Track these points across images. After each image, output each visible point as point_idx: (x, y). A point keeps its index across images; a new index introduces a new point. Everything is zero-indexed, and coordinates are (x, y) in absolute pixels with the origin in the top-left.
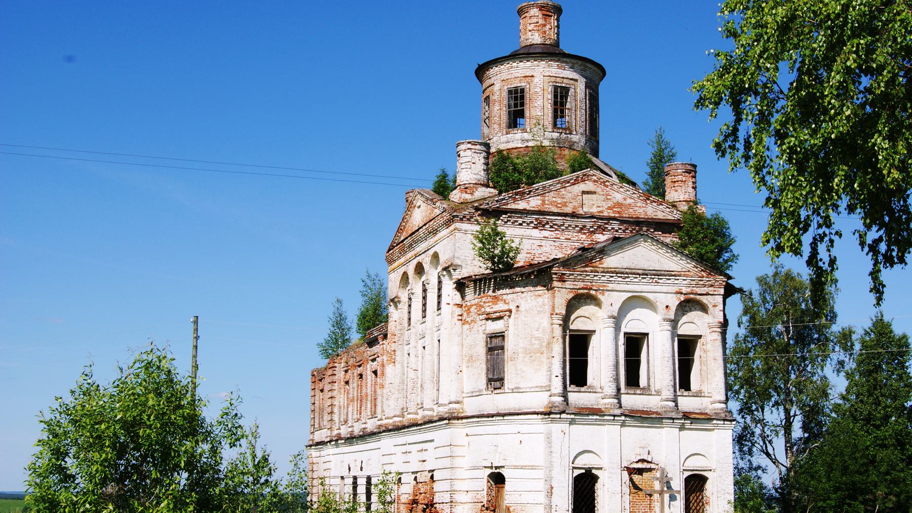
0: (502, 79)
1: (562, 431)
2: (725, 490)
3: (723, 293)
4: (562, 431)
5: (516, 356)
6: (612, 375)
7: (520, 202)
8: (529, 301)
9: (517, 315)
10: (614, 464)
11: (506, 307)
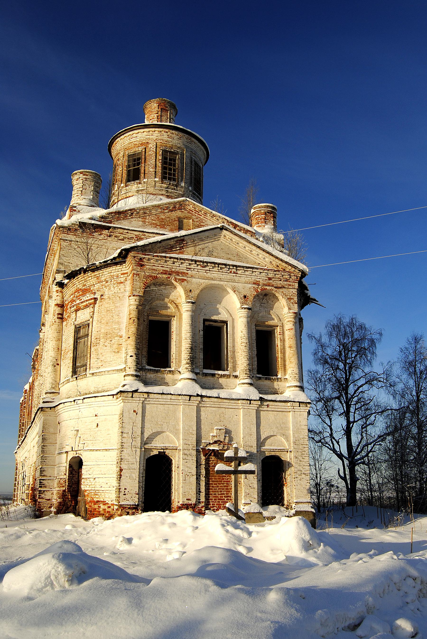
0: (345, 566)
1: (134, 411)
2: (301, 471)
3: (297, 288)
4: (134, 411)
5: (98, 342)
6: (189, 357)
7: (123, 221)
8: (112, 289)
9: (101, 303)
10: (189, 445)
11: (92, 296)
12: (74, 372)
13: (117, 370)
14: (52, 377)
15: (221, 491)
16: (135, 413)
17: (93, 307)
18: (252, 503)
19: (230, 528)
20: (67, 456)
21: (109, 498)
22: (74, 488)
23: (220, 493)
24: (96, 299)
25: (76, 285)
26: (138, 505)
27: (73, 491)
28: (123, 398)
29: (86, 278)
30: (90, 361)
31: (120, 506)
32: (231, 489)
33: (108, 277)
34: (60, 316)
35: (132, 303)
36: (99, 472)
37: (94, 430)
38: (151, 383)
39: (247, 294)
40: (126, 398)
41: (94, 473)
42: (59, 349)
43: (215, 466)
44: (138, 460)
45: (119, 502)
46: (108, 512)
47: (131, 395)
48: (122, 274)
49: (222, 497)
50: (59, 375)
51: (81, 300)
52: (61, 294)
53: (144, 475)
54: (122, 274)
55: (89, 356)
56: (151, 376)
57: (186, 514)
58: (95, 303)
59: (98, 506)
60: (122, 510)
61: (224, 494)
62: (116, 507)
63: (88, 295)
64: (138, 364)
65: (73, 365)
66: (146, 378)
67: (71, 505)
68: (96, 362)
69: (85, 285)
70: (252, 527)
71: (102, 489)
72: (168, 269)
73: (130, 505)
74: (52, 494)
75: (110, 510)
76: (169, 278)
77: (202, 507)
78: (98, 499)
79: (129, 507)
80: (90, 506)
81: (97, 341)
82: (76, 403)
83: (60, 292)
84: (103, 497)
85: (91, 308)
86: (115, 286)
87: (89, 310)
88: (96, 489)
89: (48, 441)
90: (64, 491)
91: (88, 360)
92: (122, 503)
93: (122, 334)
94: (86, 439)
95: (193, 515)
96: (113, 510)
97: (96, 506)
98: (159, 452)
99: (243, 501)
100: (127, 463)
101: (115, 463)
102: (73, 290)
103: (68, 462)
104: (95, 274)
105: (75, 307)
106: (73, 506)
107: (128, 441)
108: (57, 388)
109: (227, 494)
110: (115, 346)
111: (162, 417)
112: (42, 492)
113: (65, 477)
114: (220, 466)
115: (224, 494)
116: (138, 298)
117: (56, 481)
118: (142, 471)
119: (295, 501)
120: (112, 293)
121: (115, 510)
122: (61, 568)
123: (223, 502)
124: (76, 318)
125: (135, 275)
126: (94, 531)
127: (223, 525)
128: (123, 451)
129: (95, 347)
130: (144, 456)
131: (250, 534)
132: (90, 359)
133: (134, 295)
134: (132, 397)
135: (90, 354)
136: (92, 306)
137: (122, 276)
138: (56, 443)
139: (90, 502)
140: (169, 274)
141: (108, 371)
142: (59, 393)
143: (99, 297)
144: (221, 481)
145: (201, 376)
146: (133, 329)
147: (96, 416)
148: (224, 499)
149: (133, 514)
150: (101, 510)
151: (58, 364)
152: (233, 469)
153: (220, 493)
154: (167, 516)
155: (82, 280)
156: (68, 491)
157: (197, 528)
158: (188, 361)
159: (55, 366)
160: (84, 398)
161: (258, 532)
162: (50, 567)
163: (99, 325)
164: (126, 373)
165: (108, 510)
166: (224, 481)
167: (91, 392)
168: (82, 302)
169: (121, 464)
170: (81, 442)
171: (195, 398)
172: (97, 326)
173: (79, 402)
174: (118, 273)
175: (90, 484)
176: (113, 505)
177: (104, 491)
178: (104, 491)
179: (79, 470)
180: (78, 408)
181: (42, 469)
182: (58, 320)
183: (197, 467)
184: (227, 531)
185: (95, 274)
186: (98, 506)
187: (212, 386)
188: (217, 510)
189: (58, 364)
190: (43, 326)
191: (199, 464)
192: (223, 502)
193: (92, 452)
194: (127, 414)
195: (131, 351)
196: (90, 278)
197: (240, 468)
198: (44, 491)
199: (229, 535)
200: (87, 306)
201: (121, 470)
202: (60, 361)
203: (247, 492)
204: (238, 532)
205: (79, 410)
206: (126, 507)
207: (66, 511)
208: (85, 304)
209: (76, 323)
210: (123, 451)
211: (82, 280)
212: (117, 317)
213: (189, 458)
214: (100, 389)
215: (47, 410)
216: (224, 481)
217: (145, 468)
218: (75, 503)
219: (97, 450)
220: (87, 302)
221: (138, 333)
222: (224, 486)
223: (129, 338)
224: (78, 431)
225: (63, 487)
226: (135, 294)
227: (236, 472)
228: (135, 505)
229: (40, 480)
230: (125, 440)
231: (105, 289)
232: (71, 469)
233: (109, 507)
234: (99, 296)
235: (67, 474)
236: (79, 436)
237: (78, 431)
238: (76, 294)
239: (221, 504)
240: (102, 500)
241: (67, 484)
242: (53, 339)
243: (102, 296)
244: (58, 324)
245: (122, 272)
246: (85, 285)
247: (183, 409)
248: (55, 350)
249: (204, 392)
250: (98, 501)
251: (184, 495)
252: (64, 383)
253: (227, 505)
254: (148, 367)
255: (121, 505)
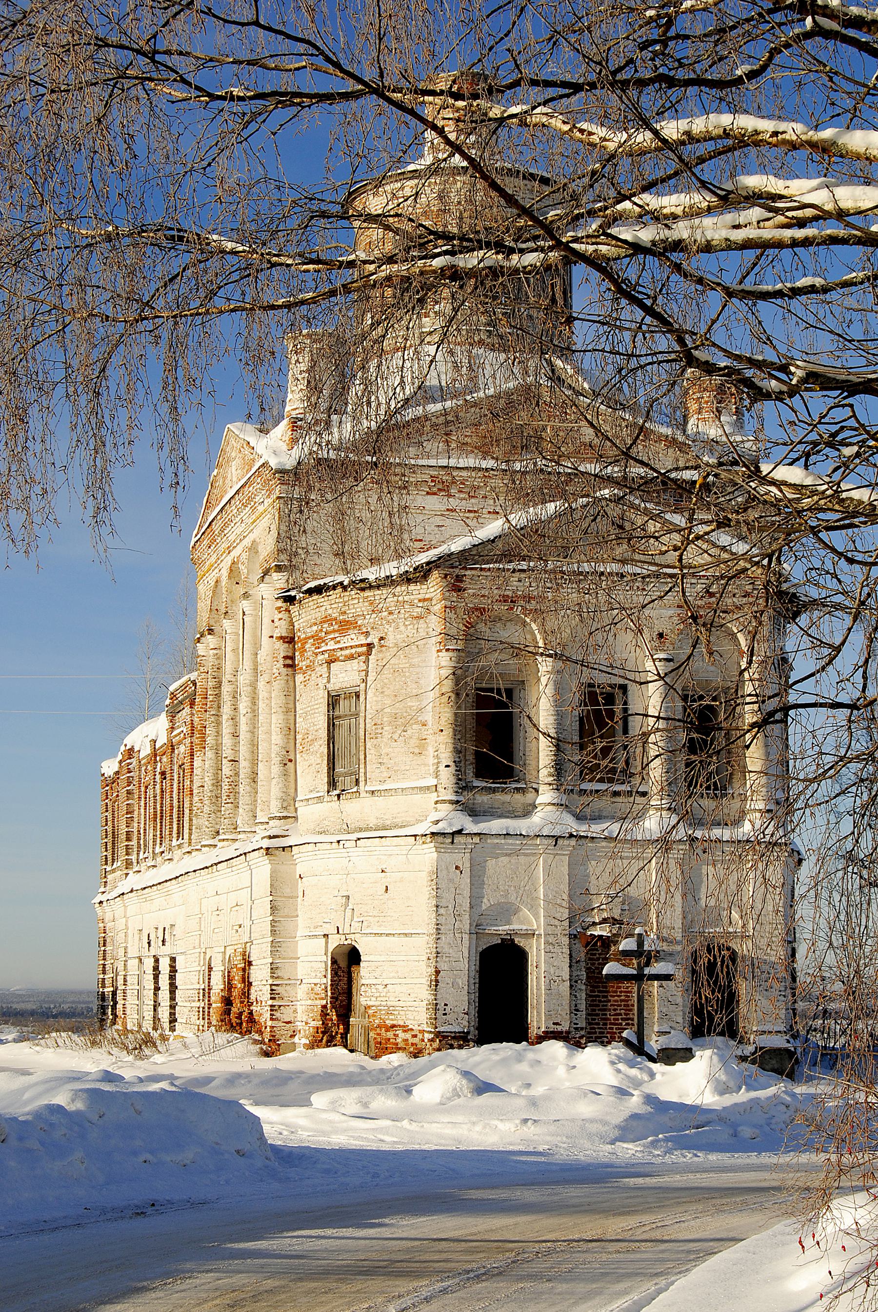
4: (457, 868)
5: (380, 731)
9: (381, 655)
10: (556, 926)
12: (332, 783)
13: (421, 788)
14: (280, 785)
15: (615, 1010)
16: (458, 872)
17: (367, 662)
18: (672, 1031)
19: (621, 1066)
20: (327, 943)
21: (414, 1020)
22: (341, 1002)
23: (613, 1012)
24: (370, 646)
25: (324, 608)
26: (468, 1033)
27: (340, 1006)
28: (437, 845)
29: (346, 599)
30: (365, 767)
31: (438, 1034)
32: (633, 1005)
33: (393, 604)
34: (289, 662)
35: (443, 664)
36: (392, 975)
37: (381, 897)
38: (484, 812)
39: (665, 630)
40: (442, 846)
41: (384, 975)
42: (291, 731)
43: (602, 969)
44: (466, 954)
45: (436, 1028)
46: (412, 1044)
47: (450, 840)
48: (420, 601)
49: (618, 1019)
50: (293, 782)
51: (339, 642)
52: (287, 615)
53: (477, 981)
54: (420, 601)
55: (362, 757)
56: (483, 799)
57: (556, 1048)
58: (369, 653)
59: (394, 1035)
60: (440, 1041)
61: (620, 1014)
62: (428, 1036)
63: (353, 636)
64: (460, 780)
65: (329, 769)
66: (474, 804)
67: (337, 1033)
68: (377, 771)
69: (345, 612)
70: (656, 1067)
71: (401, 1004)
72: (509, 593)
73: (455, 1032)
74: (295, 1011)
75: (415, 1040)
76: (512, 609)
77: (581, 1037)
78: (395, 1022)
79: (453, 1035)
80: (379, 1034)
81: (376, 729)
82: (341, 846)
83: (286, 610)
84: (404, 1017)
85: (362, 663)
86: (407, 623)
87: (356, 665)
88: (389, 1003)
89: (282, 911)
90: (324, 1007)
91: (362, 766)
92: (442, 1029)
93: (426, 719)
94: (366, 914)
95: (567, 1048)
96: (423, 1040)
97: (390, 1034)
98: (502, 939)
99: (656, 1029)
100: (447, 959)
101: (425, 958)
102: (319, 615)
103: (329, 955)
104: (366, 595)
105: (326, 655)
106: (341, 1034)
107: (448, 921)
108: (292, 808)
109: (626, 1014)
110: (414, 742)
111: (507, 877)
112: (277, 1007)
113: (324, 981)
114: (610, 968)
115: (620, 1014)
116: (455, 654)
117: (304, 987)
118: (473, 974)
119: (755, 1029)
120: (402, 636)
121: (426, 1040)
122: (464, 1082)
123: (619, 1029)
124: (329, 677)
125: (448, 610)
126: (399, 1074)
127: (613, 1063)
128: (439, 938)
129: (375, 741)
130: (477, 947)
131: (652, 1075)
132: (365, 762)
133: (447, 650)
134: (452, 843)
135: (365, 754)
136: (363, 658)
137: (420, 604)
138: (297, 916)
139: (379, 1026)
140: (512, 601)
141: (403, 789)
142: (296, 818)
143: (376, 641)
144: (616, 992)
145: (576, 796)
146: (447, 715)
147: (383, 871)
148: (621, 1024)
149: (460, 1047)
150: (399, 1040)
151: (290, 761)
152: (635, 972)
153: (613, 1012)
154: (525, 1050)
155: (337, 600)
156: (333, 1007)
157: (574, 1067)
158: (552, 770)
159: (285, 764)
160: (359, 839)
161: (663, 1074)
162: (455, 1081)
163: (379, 699)
164: (438, 796)
165: (411, 1040)
166: (621, 992)
167: (371, 825)
168: (341, 649)
169: (437, 962)
170: (356, 919)
171: (566, 842)
172: (375, 699)
173: (348, 844)
174: (412, 597)
175: (378, 994)
176: (422, 1032)
177: (405, 1009)
178: (405, 1009)
179: (349, 967)
180: (346, 855)
181: (274, 966)
182: (284, 671)
183: (570, 967)
184: (619, 1071)
185: (366, 595)
186: (394, 1035)
187: (597, 814)
188: (609, 1043)
189: (290, 761)
190: (209, 634)
191: (574, 961)
192: (619, 1029)
193: (378, 938)
194: (445, 872)
195: (446, 756)
196: (356, 601)
197: (647, 971)
198: (280, 1006)
199: (621, 1075)
200: (351, 657)
201: (437, 972)
202: (293, 753)
203: (664, 1011)
204: (634, 1072)
205: (348, 859)
206: (448, 1036)
207: (330, 1043)
208: (347, 652)
209: (330, 687)
210: (439, 938)
211: (337, 600)
212: (414, 686)
213: (557, 949)
214: (388, 822)
215: (277, 852)
216: (621, 992)
217: (478, 968)
218: (344, 1029)
219: (387, 935)
220: (353, 651)
221: (456, 720)
222: (622, 1001)
223: (442, 731)
224: (348, 897)
225: (323, 999)
226: (450, 647)
227: (639, 978)
228: (463, 1032)
229: (271, 985)
230: (442, 920)
231: (387, 627)
232: (336, 966)
233: (415, 1036)
234: (377, 640)
235: (329, 976)
236: (351, 907)
237: (348, 897)
238: (326, 625)
239: (615, 1033)
240: (402, 1023)
241: (329, 994)
242: (279, 709)
243: (382, 639)
244: (286, 678)
245: (420, 596)
246: (345, 612)
247: (545, 861)
248: (284, 733)
249: (582, 829)
250: (393, 1026)
251: (548, 1016)
252: (310, 802)
253: (624, 1035)
254: (477, 783)
255: (439, 1032)
